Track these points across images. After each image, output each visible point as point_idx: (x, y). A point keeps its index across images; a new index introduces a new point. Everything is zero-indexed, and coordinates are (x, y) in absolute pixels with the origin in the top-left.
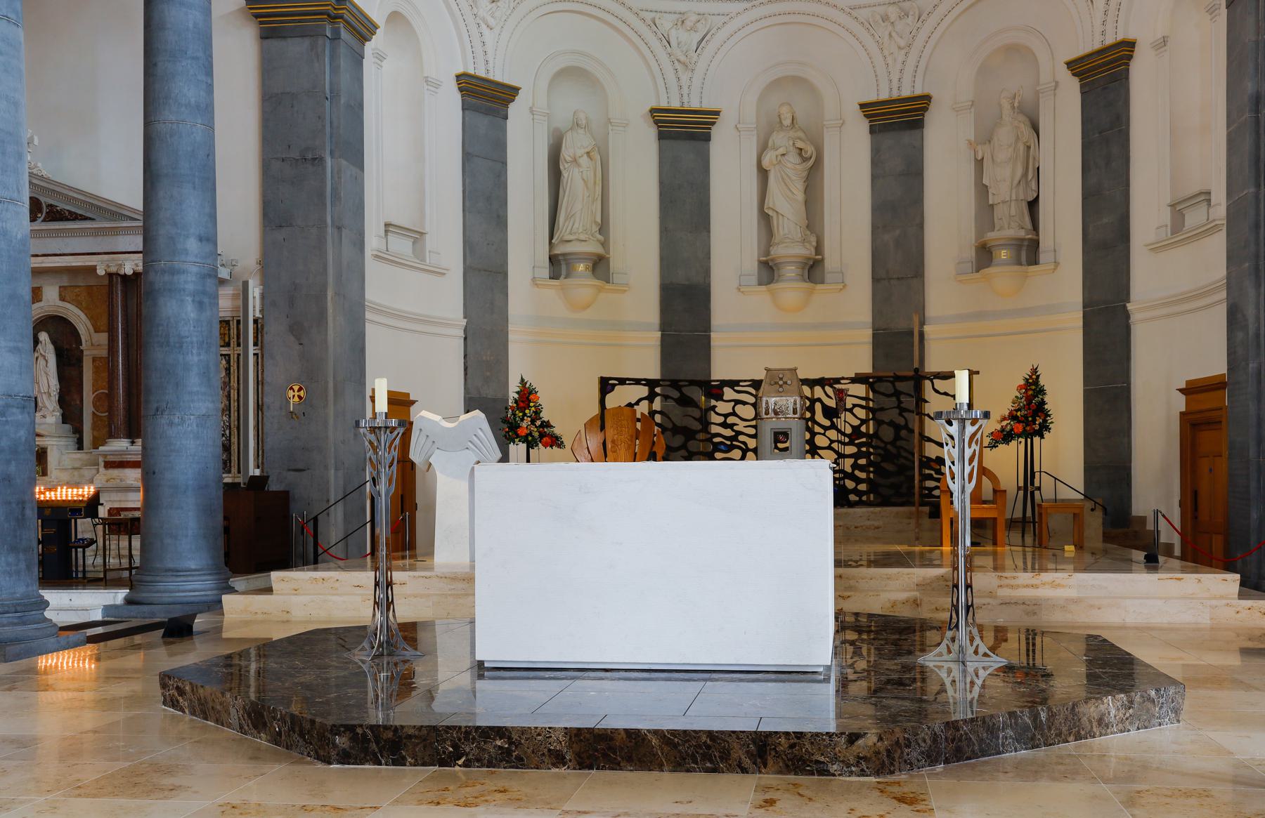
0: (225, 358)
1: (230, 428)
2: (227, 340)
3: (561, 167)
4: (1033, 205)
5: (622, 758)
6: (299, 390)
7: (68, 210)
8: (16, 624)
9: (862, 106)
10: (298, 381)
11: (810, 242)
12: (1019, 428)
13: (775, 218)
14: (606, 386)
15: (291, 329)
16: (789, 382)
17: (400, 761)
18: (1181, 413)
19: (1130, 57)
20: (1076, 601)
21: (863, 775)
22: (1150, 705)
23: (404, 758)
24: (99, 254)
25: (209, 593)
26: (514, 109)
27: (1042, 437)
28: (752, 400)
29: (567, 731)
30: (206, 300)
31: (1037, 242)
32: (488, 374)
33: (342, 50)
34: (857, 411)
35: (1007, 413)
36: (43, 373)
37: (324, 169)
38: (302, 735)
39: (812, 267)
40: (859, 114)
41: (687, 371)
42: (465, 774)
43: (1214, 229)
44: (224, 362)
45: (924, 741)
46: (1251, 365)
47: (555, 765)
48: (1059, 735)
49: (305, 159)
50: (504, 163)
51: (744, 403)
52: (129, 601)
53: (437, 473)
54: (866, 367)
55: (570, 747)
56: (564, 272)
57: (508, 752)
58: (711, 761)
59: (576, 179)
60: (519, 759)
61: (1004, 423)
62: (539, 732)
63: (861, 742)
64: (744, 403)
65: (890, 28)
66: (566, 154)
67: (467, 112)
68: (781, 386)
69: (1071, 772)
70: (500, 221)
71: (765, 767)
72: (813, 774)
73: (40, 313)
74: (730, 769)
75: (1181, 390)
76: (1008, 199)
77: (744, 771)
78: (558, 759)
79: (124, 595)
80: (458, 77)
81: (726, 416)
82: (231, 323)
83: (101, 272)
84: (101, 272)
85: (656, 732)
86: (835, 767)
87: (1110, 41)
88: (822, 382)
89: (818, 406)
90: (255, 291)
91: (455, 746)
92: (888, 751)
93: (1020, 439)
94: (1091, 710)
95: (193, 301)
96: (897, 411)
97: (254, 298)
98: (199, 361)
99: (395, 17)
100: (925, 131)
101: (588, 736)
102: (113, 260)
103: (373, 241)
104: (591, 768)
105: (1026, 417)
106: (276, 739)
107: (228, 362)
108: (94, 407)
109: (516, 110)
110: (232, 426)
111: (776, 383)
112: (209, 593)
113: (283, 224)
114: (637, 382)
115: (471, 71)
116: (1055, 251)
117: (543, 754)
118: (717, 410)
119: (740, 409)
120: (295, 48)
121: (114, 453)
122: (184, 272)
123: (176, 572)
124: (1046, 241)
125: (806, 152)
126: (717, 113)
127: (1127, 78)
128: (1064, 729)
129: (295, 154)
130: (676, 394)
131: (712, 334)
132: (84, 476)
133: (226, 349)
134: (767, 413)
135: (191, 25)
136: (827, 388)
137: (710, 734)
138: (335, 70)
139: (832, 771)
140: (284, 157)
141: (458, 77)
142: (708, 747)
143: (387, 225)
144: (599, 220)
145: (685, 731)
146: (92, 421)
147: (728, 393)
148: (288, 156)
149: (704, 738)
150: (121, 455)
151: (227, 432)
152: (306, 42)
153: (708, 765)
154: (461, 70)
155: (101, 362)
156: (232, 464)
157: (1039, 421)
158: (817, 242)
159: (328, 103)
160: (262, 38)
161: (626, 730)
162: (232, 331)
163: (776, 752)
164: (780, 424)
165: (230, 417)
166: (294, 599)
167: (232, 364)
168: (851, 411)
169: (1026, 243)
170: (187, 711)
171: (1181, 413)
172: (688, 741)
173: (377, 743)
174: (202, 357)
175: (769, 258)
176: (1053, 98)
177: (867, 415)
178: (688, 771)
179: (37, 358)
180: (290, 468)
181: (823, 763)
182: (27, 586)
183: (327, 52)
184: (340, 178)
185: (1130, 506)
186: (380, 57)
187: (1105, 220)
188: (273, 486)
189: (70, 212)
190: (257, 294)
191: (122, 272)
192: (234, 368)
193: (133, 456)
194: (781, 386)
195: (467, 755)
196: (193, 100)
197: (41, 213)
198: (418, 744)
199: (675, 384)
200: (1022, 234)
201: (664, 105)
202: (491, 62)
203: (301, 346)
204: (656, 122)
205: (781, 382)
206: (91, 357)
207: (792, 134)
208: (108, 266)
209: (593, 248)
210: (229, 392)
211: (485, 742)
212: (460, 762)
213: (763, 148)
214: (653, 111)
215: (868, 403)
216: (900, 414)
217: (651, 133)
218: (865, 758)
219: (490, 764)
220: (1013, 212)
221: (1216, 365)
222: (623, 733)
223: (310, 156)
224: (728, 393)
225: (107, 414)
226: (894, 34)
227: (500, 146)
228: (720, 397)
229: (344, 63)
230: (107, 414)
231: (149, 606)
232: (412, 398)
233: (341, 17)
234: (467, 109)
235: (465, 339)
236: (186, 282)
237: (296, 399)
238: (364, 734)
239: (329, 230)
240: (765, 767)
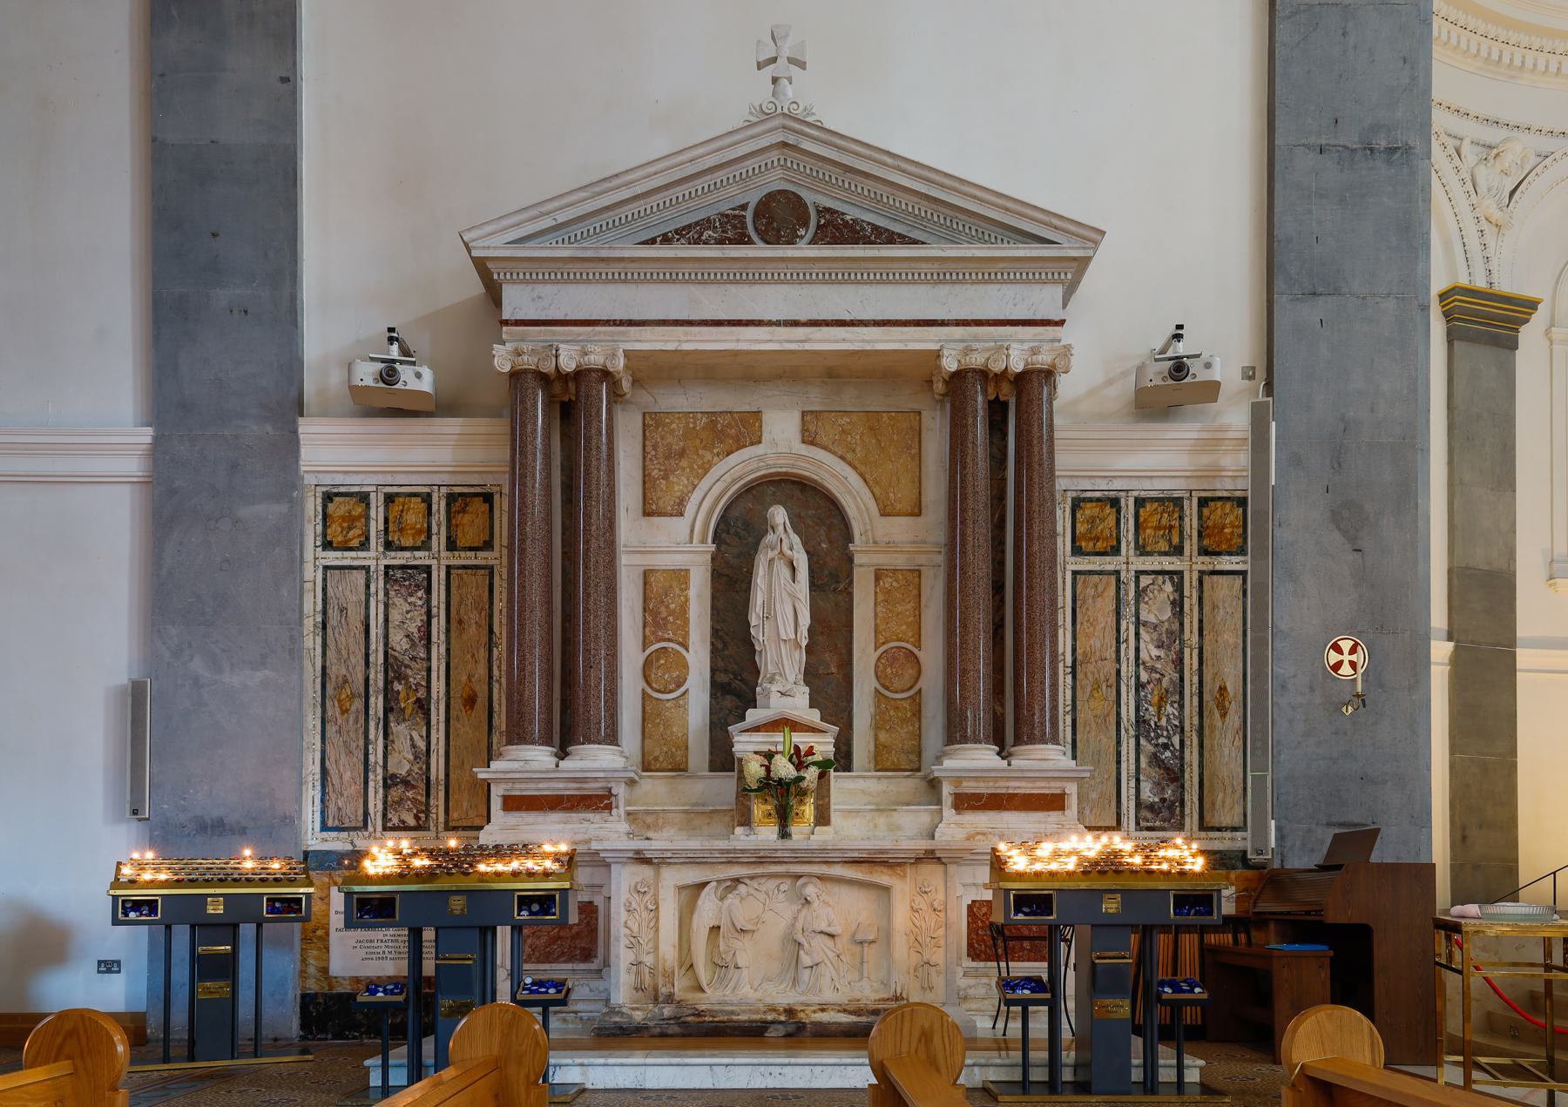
0: (1171, 580)
1: (1182, 731)
2: (1176, 540)
7: (869, 223)
10: (1350, 629)
15: (1336, 518)
24: (943, 323)
36: (784, 595)
44: (1168, 588)
49: (1372, 150)
73: (758, 469)
82: (1186, 503)
107: (1179, 588)
108: (878, 678)
110: (1187, 728)
113: (1320, 290)
129: (1351, 138)
132: (899, 828)
133: (1174, 559)
140: (1324, 142)
148: (1332, 142)
150: (996, 779)
151: (1176, 740)
155: (896, 580)
156: (1187, 811)
162: (1187, 520)
165: (1182, 707)
167: (1186, 593)
179: (771, 561)
180: (1334, 820)
189: (875, 228)
192: (1190, 603)
193: (1023, 784)
203: (1357, 556)
206: (872, 569)
210: (1181, 652)
223: (1383, 144)
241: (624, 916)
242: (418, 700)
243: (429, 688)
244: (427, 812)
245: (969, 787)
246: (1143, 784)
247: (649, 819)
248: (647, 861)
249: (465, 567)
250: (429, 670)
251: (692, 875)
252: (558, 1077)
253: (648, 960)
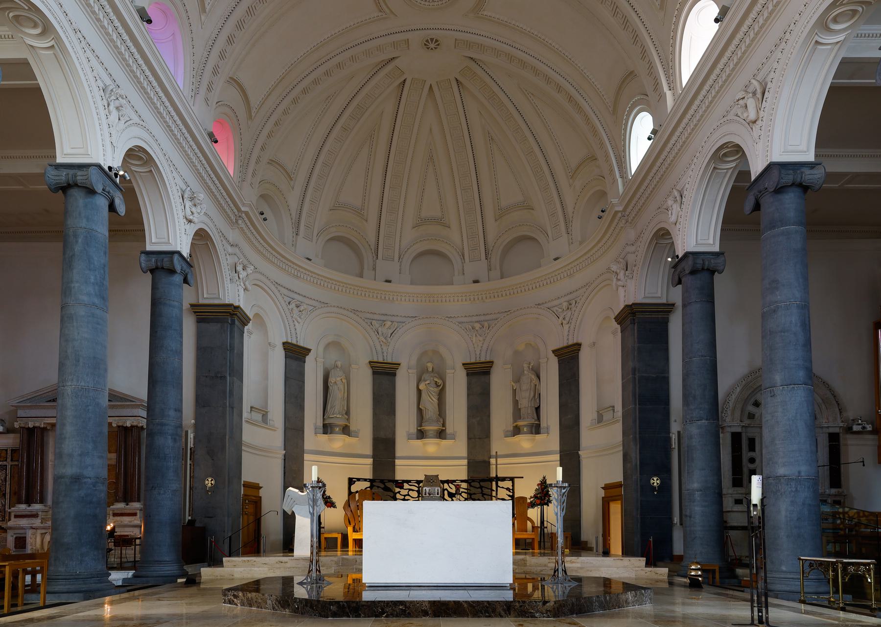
3: (329, 385)
4: (538, 409)
5: (452, 613)
8: (97, 583)
9: (463, 364)
11: (440, 421)
12: (538, 502)
13: (424, 410)
14: (351, 481)
16: (435, 481)
17: (358, 616)
18: (603, 498)
19: (579, 350)
20: (581, 568)
21: (549, 617)
22: (642, 596)
23: (360, 615)
25: (175, 572)
26: (308, 359)
27: (548, 505)
28: (417, 489)
29: (430, 602)
30: (178, 438)
31: (540, 424)
32: (295, 475)
33: (236, 329)
34: (463, 494)
35: (533, 495)
37: (226, 381)
38: (311, 607)
39: (440, 432)
40: (462, 368)
41: (386, 476)
42: (386, 620)
43: (617, 421)
45: (569, 605)
46: (634, 477)
47: (424, 616)
48: (613, 606)
50: (304, 382)
51: (413, 490)
52: (134, 576)
53: (296, 515)
54: (465, 477)
55: (430, 608)
56: (329, 431)
57: (405, 611)
58: (488, 613)
59: (337, 393)
60: (409, 614)
61: (532, 499)
62: (418, 602)
63: (548, 604)
64: (413, 490)
65: (476, 332)
66: (332, 380)
67: (287, 359)
68: (431, 483)
69: (626, 616)
70: (302, 408)
71: (510, 615)
72: (529, 617)
74: (496, 616)
75: (602, 488)
76: (527, 406)
77: (501, 616)
78: (425, 613)
79: (132, 574)
80: (284, 343)
81: (405, 496)
83: (114, 425)
84: (114, 425)
85: (466, 602)
86: (538, 614)
87: (570, 343)
88: (448, 482)
89: (446, 492)
90: (191, 436)
91: (382, 609)
92: (557, 608)
93: (539, 506)
94: (623, 597)
95: (172, 438)
96: (481, 495)
97: (191, 438)
98: (174, 465)
99: (257, 315)
100: (396, 377)
101: (438, 604)
102: (121, 420)
103: (245, 415)
104: (439, 617)
105: (540, 497)
106: (295, 611)
109: (309, 360)
111: (430, 481)
112: (175, 572)
114: (365, 480)
115: (290, 341)
116: (547, 429)
117: (419, 612)
118: (401, 493)
119: (411, 493)
120: (214, 327)
121: (118, 509)
122: (167, 425)
123: (160, 562)
124: (543, 424)
125: (439, 383)
126: (399, 364)
127: (578, 358)
128: (615, 604)
130: (382, 486)
131: (396, 460)
134: (425, 494)
135: (174, 315)
136: (450, 484)
137: (488, 602)
138: (232, 337)
139: (536, 616)
141: (284, 343)
142: (487, 607)
143: (251, 408)
144: (346, 409)
145: (478, 601)
147: (406, 486)
149: (486, 604)
152: (219, 325)
153: (487, 614)
154: (285, 340)
157: (547, 499)
158: (443, 422)
159: (228, 352)
160: (197, 322)
161: (454, 601)
163: (514, 609)
164: (339, 442)
166: (236, 569)
168: (460, 494)
169: (535, 425)
170: (239, 605)
171: (603, 498)
172: (479, 605)
173: (349, 609)
174: (175, 464)
175: (421, 428)
176: (546, 364)
177: (468, 496)
178: (479, 617)
181: (532, 613)
182: (102, 566)
183: (229, 330)
184: (233, 386)
185: (580, 537)
186: (250, 333)
187: (569, 416)
188: (197, 525)
190: (192, 437)
191: (125, 426)
194: (431, 483)
195: (388, 612)
196: (174, 348)
198: (366, 609)
199: (382, 481)
200: (533, 421)
201: (375, 360)
202: (299, 338)
204: (372, 367)
205: (431, 481)
207: (432, 374)
208: (118, 423)
209: (342, 422)
211: (395, 607)
212: (384, 616)
213: (419, 381)
214: (370, 362)
215: (468, 491)
216: (482, 496)
217: (369, 372)
218: (549, 611)
219: (397, 616)
220: (529, 412)
221: (618, 477)
222: (453, 603)
224: (406, 486)
225: (114, 491)
226: (477, 335)
227: (302, 374)
228: (402, 488)
229: (236, 335)
230: (114, 491)
231: (146, 578)
232: (260, 486)
233: (236, 315)
234: (288, 358)
235: (285, 460)
236: (168, 429)
237: (210, 485)
238: (344, 605)
239: (228, 409)
240: (510, 615)
241: (29, 539)
242: (3, 494)
243: (6, 490)
244: (5, 517)
245: (116, 512)
246: (735, 510)
247: (47, 519)
248: (34, 529)
249: (15, 465)
250: (6, 487)
251: (44, 531)
252: (313, 467)
253: (34, 548)
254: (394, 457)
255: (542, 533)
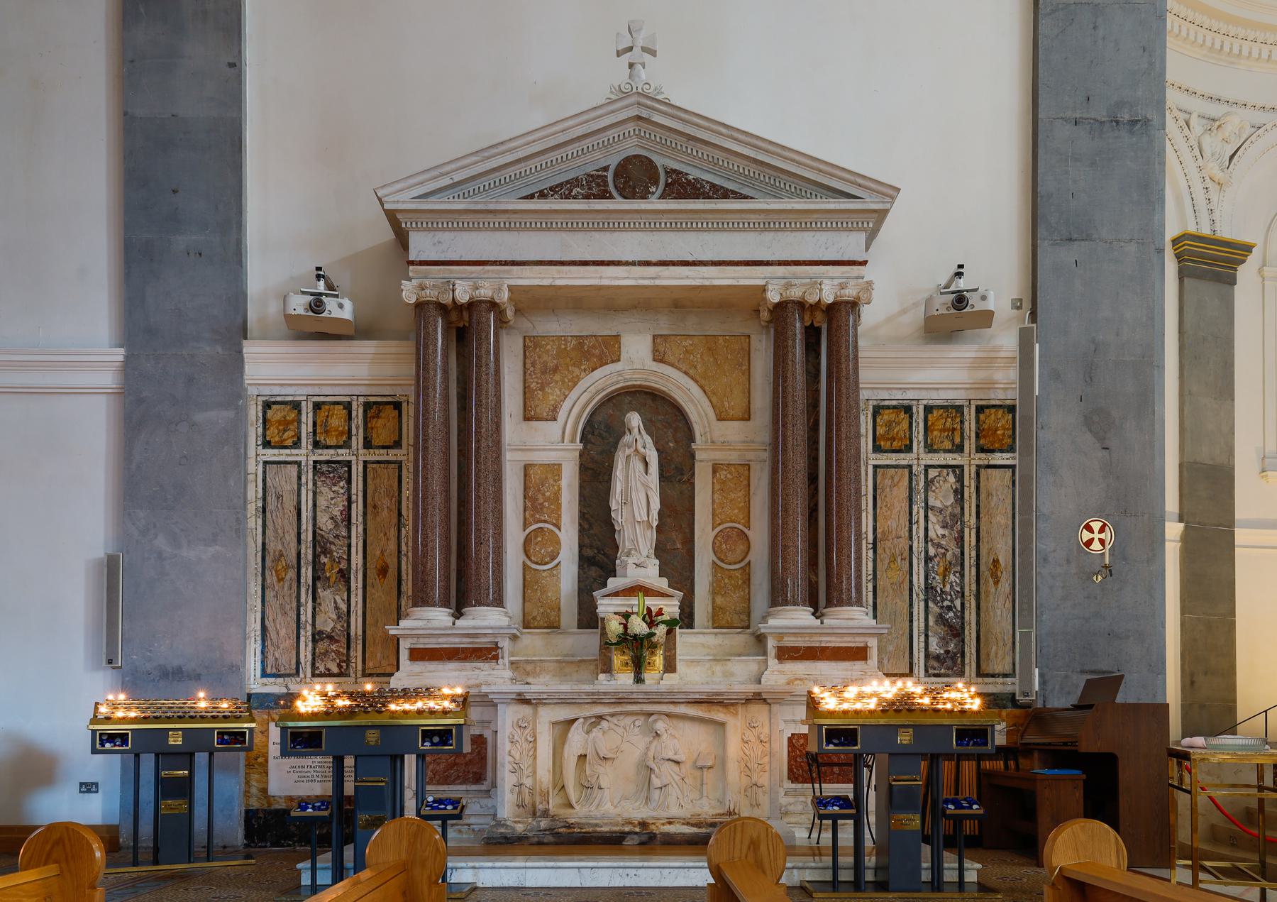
0: (954, 472)
1: (963, 595)
2: (957, 440)
6: (1102, 530)
7: (708, 182)
10: (1100, 513)
15: (1088, 422)
24: (768, 263)
36: (639, 485)
44: (952, 479)
49: (1117, 122)
73: (617, 382)
82: (966, 410)
103: (507, 447)
107: (960, 479)
108: (715, 552)
110: (967, 593)
113: (1075, 236)
129: (1100, 113)
132: (732, 675)
133: (956, 455)
140: (1078, 116)
146: (710, 578)
148: (1085, 116)
150: (811, 635)
151: (958, 603)
155: (730, 473)
156: (967, 661)
162: (967, 424)
165: (962, 576)
167: (966, 483)
180: (1086, 668)
189: (713, 186)
192: (969, 492)
193: (833, 639)
197: (656, 183)
203: (1105, 453)
206: (710, 463)
210: (962, 531)
223: (1127, 117)
241: (508, 746)
242: (341, 571)
243: (349, 560)
244: (348, 662)
245: (789, 642)
247: (529, 668)
249: (378, 462)
250: (349, 546)
251: (564, 713)
253: (528, 782)
254: (1232, 523)
255: (1192, 848)
